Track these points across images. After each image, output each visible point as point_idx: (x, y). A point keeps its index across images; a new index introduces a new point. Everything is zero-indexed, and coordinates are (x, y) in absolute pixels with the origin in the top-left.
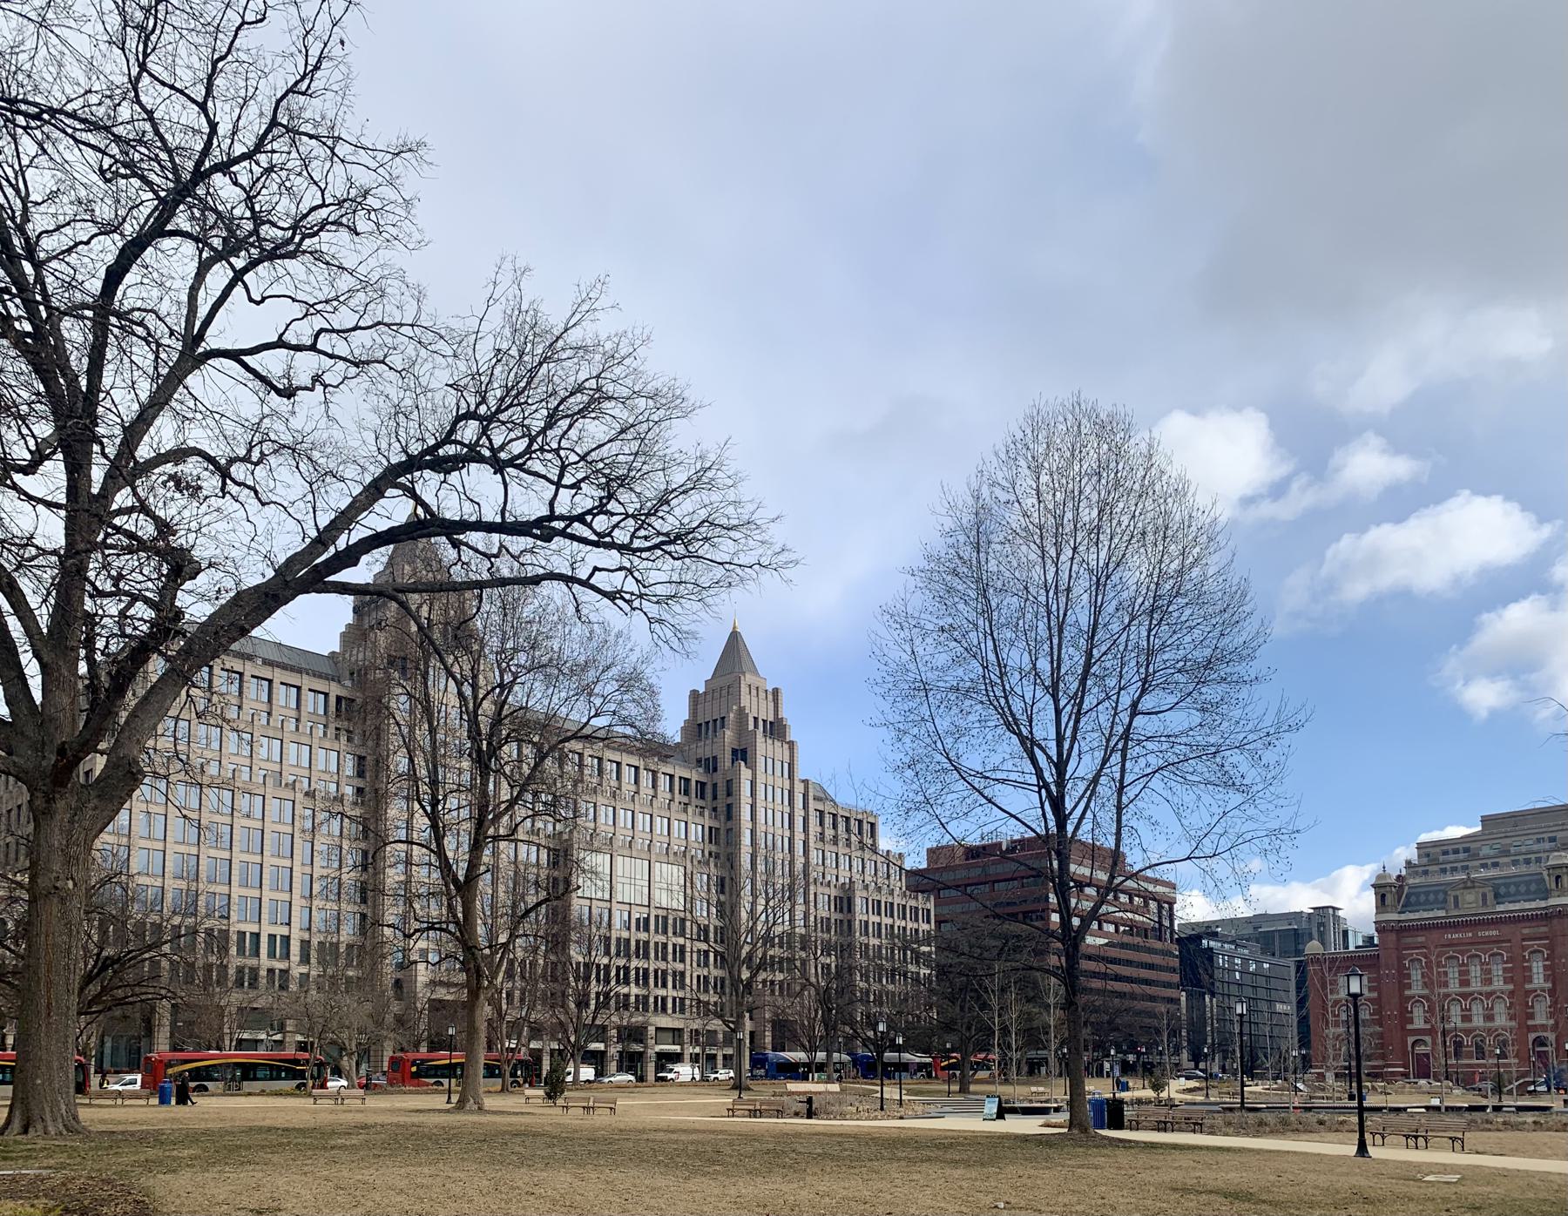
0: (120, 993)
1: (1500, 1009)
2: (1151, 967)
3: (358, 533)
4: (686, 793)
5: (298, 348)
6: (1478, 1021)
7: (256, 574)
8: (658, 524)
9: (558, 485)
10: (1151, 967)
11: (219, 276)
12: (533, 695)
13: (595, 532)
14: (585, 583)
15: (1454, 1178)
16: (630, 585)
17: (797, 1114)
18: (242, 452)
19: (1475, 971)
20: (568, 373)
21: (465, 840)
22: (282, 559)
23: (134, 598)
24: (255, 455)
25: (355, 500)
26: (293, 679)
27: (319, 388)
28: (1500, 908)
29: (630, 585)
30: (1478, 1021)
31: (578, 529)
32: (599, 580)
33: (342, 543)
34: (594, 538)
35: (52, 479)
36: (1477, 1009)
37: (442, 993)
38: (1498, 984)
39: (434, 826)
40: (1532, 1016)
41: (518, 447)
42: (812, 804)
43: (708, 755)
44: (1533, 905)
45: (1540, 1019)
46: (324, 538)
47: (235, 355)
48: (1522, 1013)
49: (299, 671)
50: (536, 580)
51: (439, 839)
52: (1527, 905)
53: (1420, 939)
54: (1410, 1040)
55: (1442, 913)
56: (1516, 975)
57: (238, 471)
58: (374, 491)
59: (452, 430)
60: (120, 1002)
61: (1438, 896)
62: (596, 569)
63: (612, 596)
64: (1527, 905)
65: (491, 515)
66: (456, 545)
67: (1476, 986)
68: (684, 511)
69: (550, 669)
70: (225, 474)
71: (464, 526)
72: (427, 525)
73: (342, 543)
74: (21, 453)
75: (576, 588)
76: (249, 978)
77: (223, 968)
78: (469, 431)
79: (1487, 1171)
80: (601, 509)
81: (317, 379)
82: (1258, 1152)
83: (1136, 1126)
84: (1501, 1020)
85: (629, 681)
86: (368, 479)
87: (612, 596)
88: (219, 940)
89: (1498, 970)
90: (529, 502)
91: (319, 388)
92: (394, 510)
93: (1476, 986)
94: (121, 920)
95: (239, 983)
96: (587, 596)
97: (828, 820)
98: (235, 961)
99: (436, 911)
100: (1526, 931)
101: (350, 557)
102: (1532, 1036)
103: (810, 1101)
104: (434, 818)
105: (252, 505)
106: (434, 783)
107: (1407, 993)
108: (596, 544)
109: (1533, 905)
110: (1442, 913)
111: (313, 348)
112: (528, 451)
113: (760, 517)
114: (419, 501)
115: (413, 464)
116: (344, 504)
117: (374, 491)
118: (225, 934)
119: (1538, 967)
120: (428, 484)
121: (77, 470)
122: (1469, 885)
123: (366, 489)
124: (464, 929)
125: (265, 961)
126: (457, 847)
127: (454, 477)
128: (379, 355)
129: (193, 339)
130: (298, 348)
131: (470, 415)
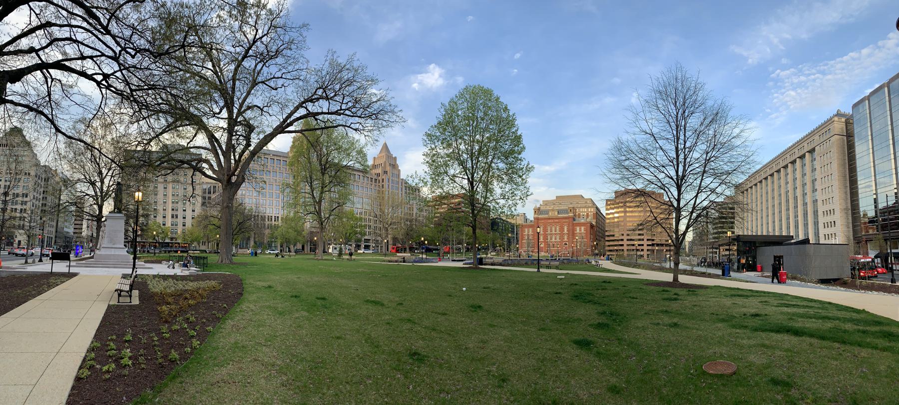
0: (243, 230)
1: (558, 237)
2: (787, 201)
3: (293, 118)
4: (372, 181)
5: (278, 78)
6: (553, 240)
7: (269, 131)
8: (368, 109)
9: (342, 103)
10: (787, 201)
11: (260, 65)
12: (335, 157)
13: (352, 113)
14: (349, 127)
15: (563, 277)
16: (361, 127)
17: (401, 262)
18: (266, 105)
19: (553, 229)
20: (346, 75)
21: (319, 193)
22: (274, 127)
23: (240, 136)
24: (269, 105)
25: (292, 111)
26: (278, 158)
27: (283, 87)
29: (361, 127)
31: (347, 112)
32: (352, 126)
33: (288, 121)
34: (352, 115)
35: (224, 114)
37: (313, 230)
39: (311, 188)
41: (332, 95)
42: (404, 185)
43: (378, 172)
45: (566, 240)
46: (285, 120)
47: (263, 82)
48: (562, 237)
49: (280, 156)
50: (336, 127)
51: (313, 191)
56: (562, 229)
57: (265, 109)
58: (297, 109)
59: (316, 92)
60: (243, 232)
61: (547, 212)
62: (352, 123)
63: (356, 130)
65: (325, 110)
66: (316, 119)
68: (376, 106)
69: (339, 149)
70: (262, 110)
71: (318, 114)
72: (310, 114)
73: (288, 121)
74: (217, 111)
75: (346, 128)
76: (270, 227)
77: (265, 224)
78: (320, 92)
79: (870, 317)
80: (354, 107)
81: (283, 85)
82: (515, 271)
83: (486, 264)
84: (558, 240)
85: (360, 152)
86: (295, 106)
87: (356, 130)
88: (263, 218)
89: (558, 228)
90: (335, 107)
91: (283, 87)
92: (302, 112)
93: (554, 232)
94: (243, 213)
95: (268, 228)
96: (349, 130)
97: (407, 189)
98: (267, 223)
99: (312, 209)
101: (291, 124)
103: (404, 258)
104: (311, 186)
105: (268, 117)
106: (311, 178)
108: (352, 116)
111: (281, 78)
112: (335, 95)
113: (396, 110)
114: (307, 110)
115: (306, 101)
116: (289, 112)
117: (297, 109)
118: (265, 216)
120: (310, 106)
121: (230, 112)
123: (295, 108)
124: (319, 213)
125: (273, 222)
126: (317, 194)
127: (316, 104)
128: (297, 77)
129: (254, 81)
130: (278, 78)
131: (320, 88)
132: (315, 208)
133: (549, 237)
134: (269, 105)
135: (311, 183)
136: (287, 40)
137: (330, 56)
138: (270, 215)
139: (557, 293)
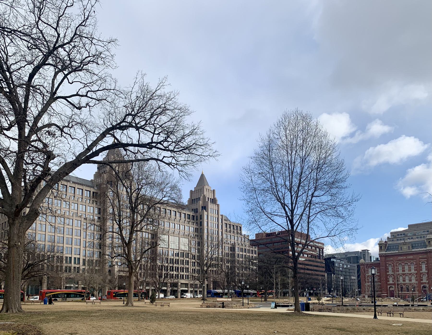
0: (33, 274)
1: (413, 278)
2: (317, 266)
3: (99, 147)
4: (189, 218)
5: (82, 96)
6: (407, 281)
7: (70, 158)
8: (181, 144)
9: (154, 134)
10: (317, 266)
13: (164, 147)
14: (161, 161)
16: (174, 161)
18: (67, 125)
19: (406, 267)
20: (157, 103)
21: (128, 231)
22: (78, 154)
24: (70, 125)
25: (98, 138)
26: (81, 187)
27: (88, 107)
28: (413, 250)
29: (174, 161)
30: (407, 281)
31: (159, 146)
32: (165, 160)
33: (94, 149)
34: (164, 148)
35: (14, 132)
36: (407, 278)
37: (122, 274)
38: (413, 271)
39: (120, 228)
40: (422, 280)
41: (143, 123)
43: (195, 208)
44: (422, 249)
45: (424, 281)
46: (89, 148)
48: (419, 279)
49: (83, 185)
50: (148, 160)
51: (121, 231)
52: (421, 249)
53: (391, 259)
54: (389, 286)
55: (397, 252)
56: (418, 269)
57: (66, 130)
58: (103, 135)
59: (125, 119)
60: (33, 276)
61: (396, 247)
62: (164, 157)
63: (169, 164)
64: (421, 249)
65: (135, 142)
66: (126, 150)
67: (407, 272)
68: (189, 141)
69: (151, 184)
70: (62, 131)
71: (128, 145)
72: (118, 145)
73: (94, 149)
75: (159, 162)
77: (62, 267)
78: (129, 119)
79: (410, 323)
80: (166, 140)
81: (87, 104)
82: (347, 317)
83: (313, 310)
84: (414, 281)
85: (173, 188)
86: (101, 132)
87: (169, 164)
88: (60, 259)
89: (413, 267)
90: (146, 138)
91: (88, 107)
92: (109, 141)
93: (407, 272)
94: (33, 254)
95: (66, 271)
96: (162, 164)
97: (228, 226)
98: (65, 265)
99: (120, 251)
100: (420, 257)
102: (422, 285)
103: (223, 303)
106: (120, 216)
107: (388, 273)
108: (164, 150)
109: (422, 249)
110: (397, 252)
111: (86, 96)
112: (145, 124)
113: (210, 142)
114: (115, 138)
115: (114, 128)
116: (95, 139)
117: (103, 135)
119: (424, 266)
121: (21, 129)
122: (405, 244)
124: (128, 256)
126: (126, 233)
127: (125, 131)
128: (105, 98)
129: (53, 93)
130: (82, 96)
131: (130, 114)
132: (124, 250)
133: (401, 279)
134: (70, 125)
135: (120, 221)
136: (93, 52)
137: (139, 77)
138: (69, 256)
139: (326, 328)
